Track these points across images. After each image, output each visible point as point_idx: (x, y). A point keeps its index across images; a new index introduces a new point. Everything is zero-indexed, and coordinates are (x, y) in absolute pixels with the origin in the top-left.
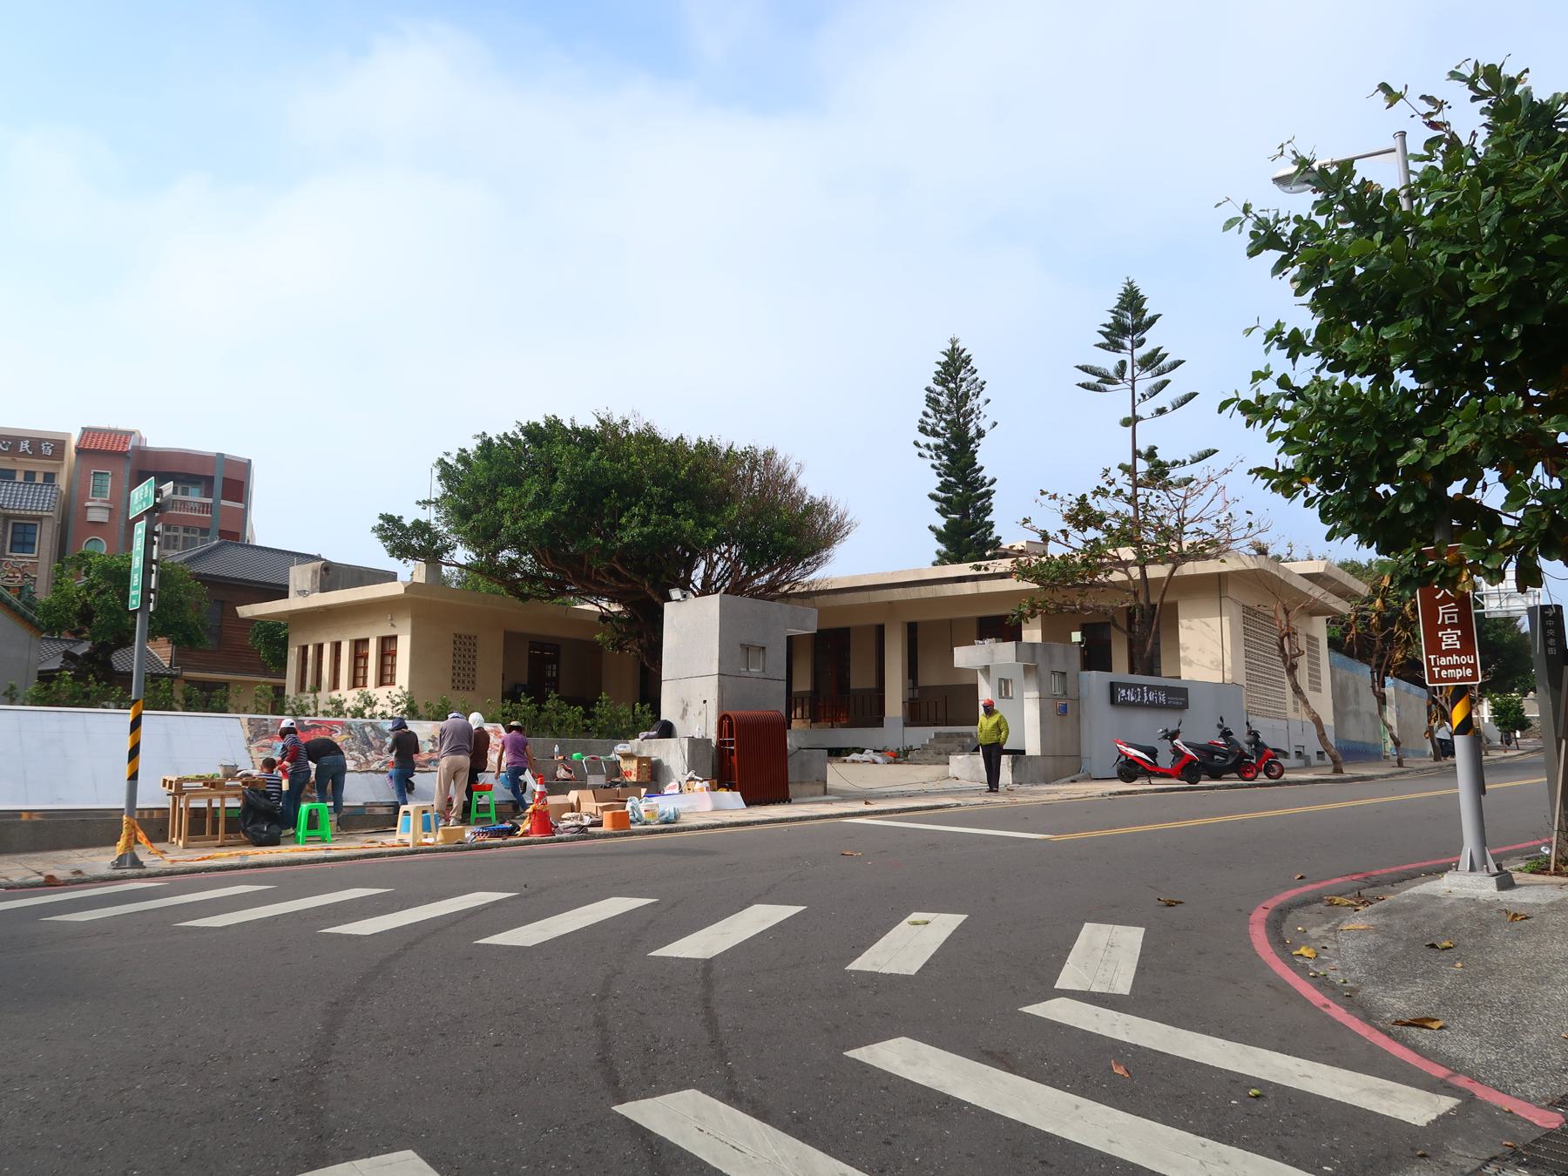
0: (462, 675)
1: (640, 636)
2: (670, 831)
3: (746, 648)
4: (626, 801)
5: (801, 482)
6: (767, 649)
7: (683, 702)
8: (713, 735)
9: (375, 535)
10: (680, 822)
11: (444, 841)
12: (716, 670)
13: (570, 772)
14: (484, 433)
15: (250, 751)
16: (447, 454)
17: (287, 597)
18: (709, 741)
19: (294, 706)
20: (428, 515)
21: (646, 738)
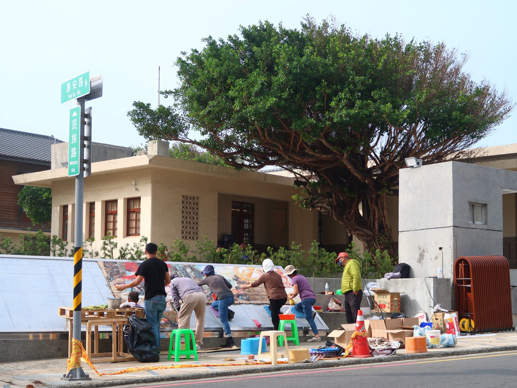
0: (188, 228)
1: (329, 195)
2: (453, 354)
3: (473, 205)
4: (413, 329)
5: (464, 70)
6: (489, 206)
7: (420, 249)
8: (449, 274)
9: (130, 117)
10: (458, 347)
11: (296, 360)
12: (450, 223)
13: (340, 305)
14: (210, 37)
15: (110, 287)
16: (184, 53)
17: (50, 169)
18: (448, 280)
19: (133, 253)
20: (169, 102)
21: (392, 278)
